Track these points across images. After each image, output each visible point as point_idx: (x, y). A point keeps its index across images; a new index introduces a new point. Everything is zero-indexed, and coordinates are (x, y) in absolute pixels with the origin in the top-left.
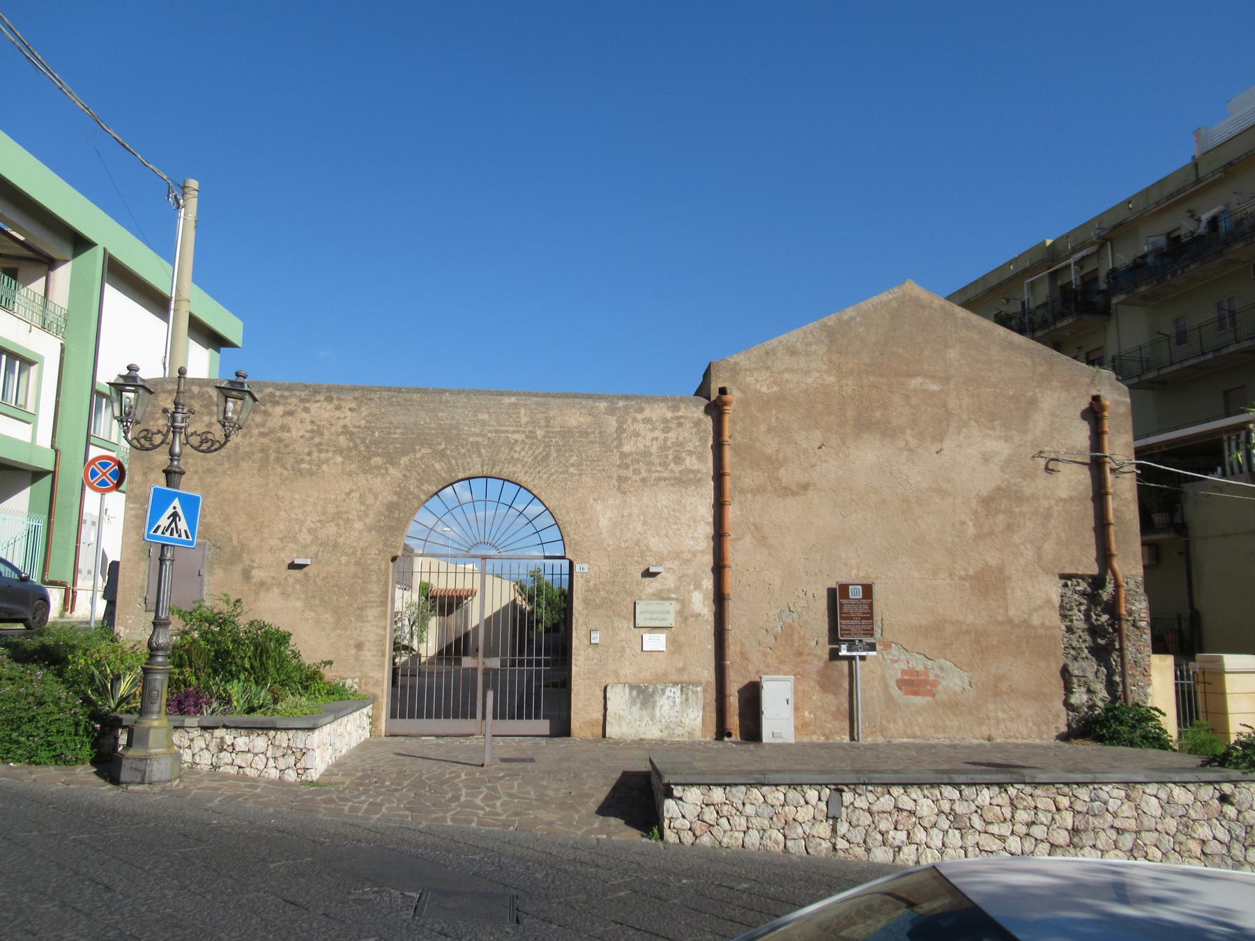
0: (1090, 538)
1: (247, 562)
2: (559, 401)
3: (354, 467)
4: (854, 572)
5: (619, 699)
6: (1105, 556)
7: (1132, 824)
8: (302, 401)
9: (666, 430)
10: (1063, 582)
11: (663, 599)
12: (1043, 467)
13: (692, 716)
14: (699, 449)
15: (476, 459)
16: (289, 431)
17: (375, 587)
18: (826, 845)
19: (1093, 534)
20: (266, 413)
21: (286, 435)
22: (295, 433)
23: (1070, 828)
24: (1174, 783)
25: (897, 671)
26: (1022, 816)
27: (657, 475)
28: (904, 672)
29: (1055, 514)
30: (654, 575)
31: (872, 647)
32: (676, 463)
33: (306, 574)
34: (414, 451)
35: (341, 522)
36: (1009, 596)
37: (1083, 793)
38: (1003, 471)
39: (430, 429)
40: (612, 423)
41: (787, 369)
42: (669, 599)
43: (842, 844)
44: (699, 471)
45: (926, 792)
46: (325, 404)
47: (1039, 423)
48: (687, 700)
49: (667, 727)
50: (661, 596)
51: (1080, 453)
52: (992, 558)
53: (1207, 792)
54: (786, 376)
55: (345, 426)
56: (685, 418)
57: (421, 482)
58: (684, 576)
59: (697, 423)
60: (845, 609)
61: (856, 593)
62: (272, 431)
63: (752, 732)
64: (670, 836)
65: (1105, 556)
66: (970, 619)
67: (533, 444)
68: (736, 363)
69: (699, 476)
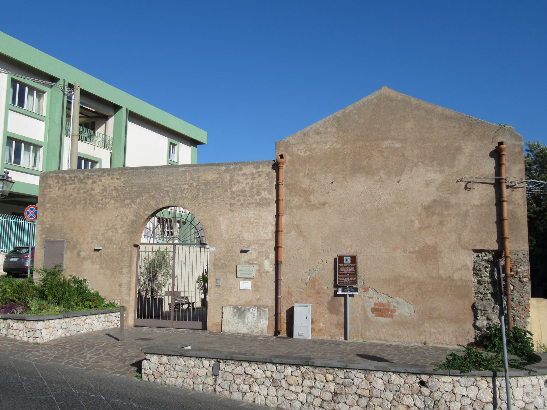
0: (494, 228)
1: (79, 249)
2: (203, 168)
3: (118, 205)
4: (348, 250)
5: (228, 313)
6: (501, 239)
7: (367, 393)
8: (99, 176)
9: (253, 178)
10: (476, 254)
11: (250, 264)
12: (464, 187)
13: (262, 323)
14: (269, 188)
15: (168, 198)
16: (94, 190)
17: (126, 259)
18: (211, 388)
19: (495, 226)
20: (86, 183)
21: (93, 192)
22: (96, 191)
23: (333, 391)
24: (393, 372)
25: (371, 304)
26: (307, 383)
27: (248, 202)
28: (375, 304)
29: (471, 214)
30: (246, 252)
31: (356, 290)
32: (257, 195)
33: (100, 254)
34: (142, 196)
35: (114, 230)
36: (440, 263)
37: (341, 374)
38: (438, 191)
39: (149, 185)
40: (227, 176)
41: (314, 142)
42: (253, 264)
43: (218, 388)
44: (269, 199)
45: (259, 366)
46: (107, 177)
47: (462, 160)
48: (260, 314)
49: (251, 328)
50: (250, 263)
51: (488, 178)
52: (430, 241)
53: (413, 379)
54: (314, 146)
55: (115, 187)
56: (262, 172)
57: (145, 210)
58: (261, 252)
59: (268, 174)
60: (341, 269)
61: (347, 261)
62: (88, 191)
63: (290, 333)
64: (144, 377)
65: (501, 239)
66: (416, 275)
67: (192, 189)
68: (288, 141)
69: (269, 201)
